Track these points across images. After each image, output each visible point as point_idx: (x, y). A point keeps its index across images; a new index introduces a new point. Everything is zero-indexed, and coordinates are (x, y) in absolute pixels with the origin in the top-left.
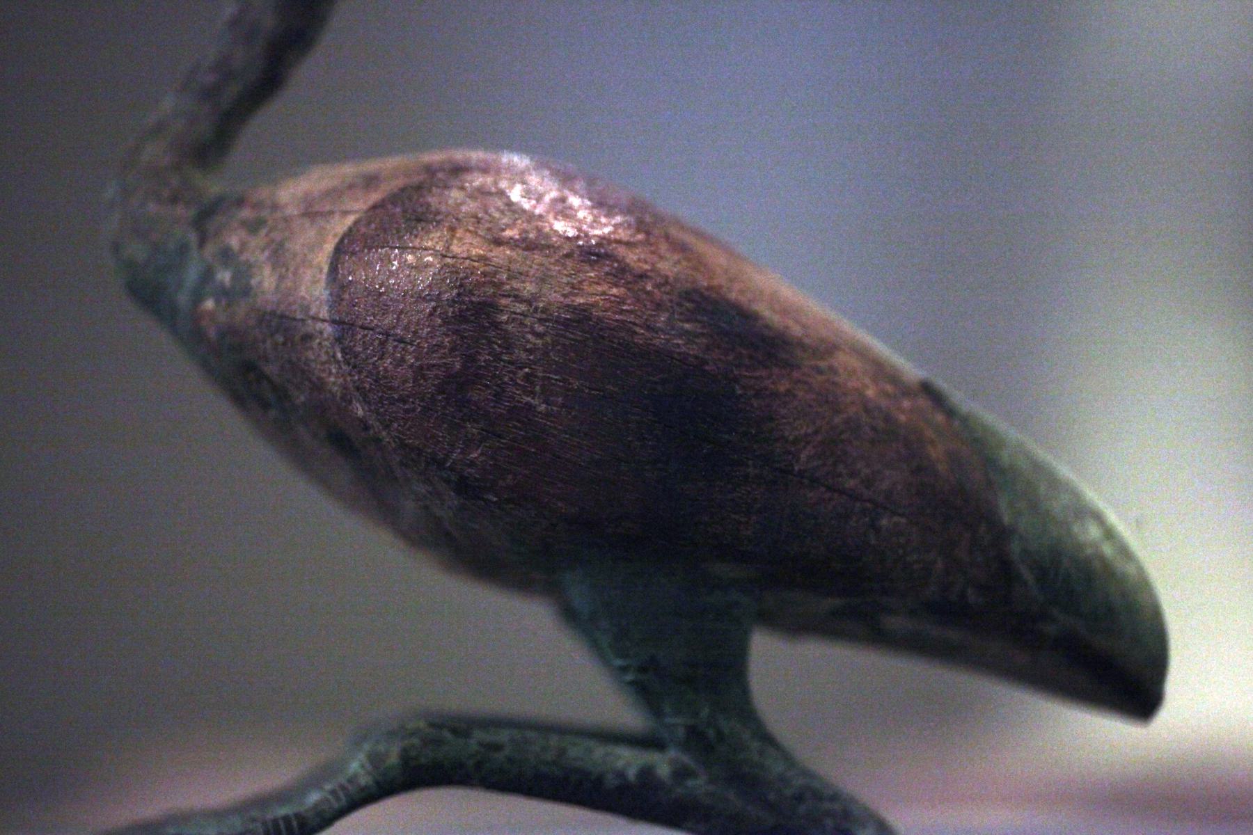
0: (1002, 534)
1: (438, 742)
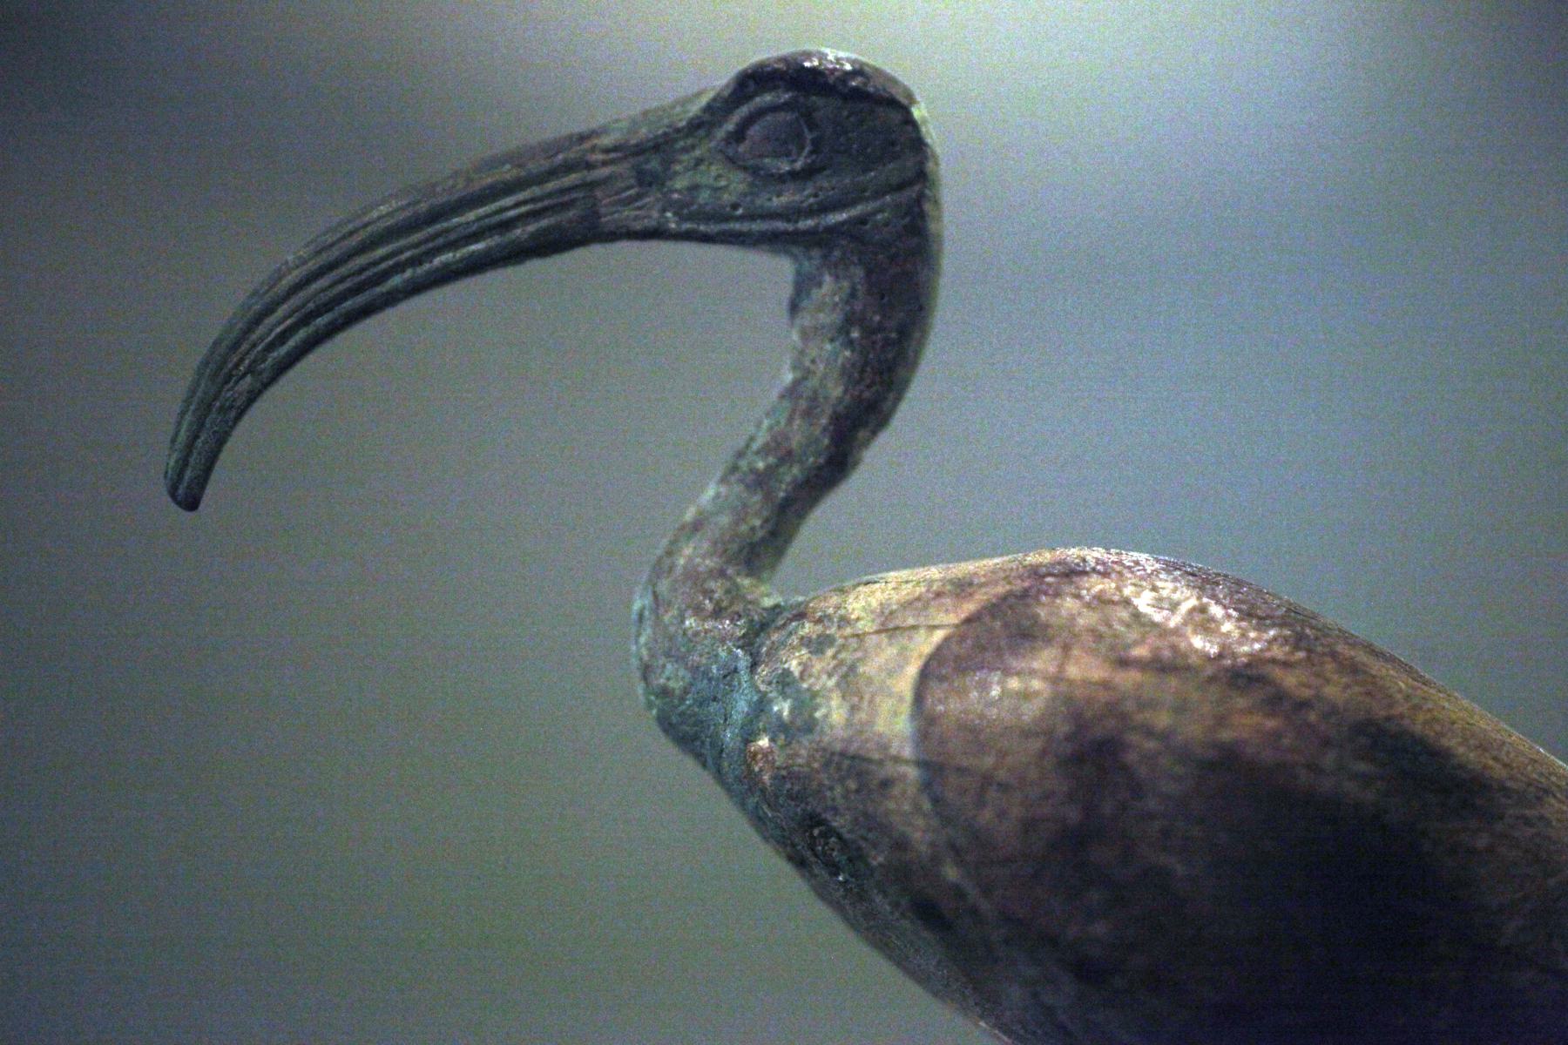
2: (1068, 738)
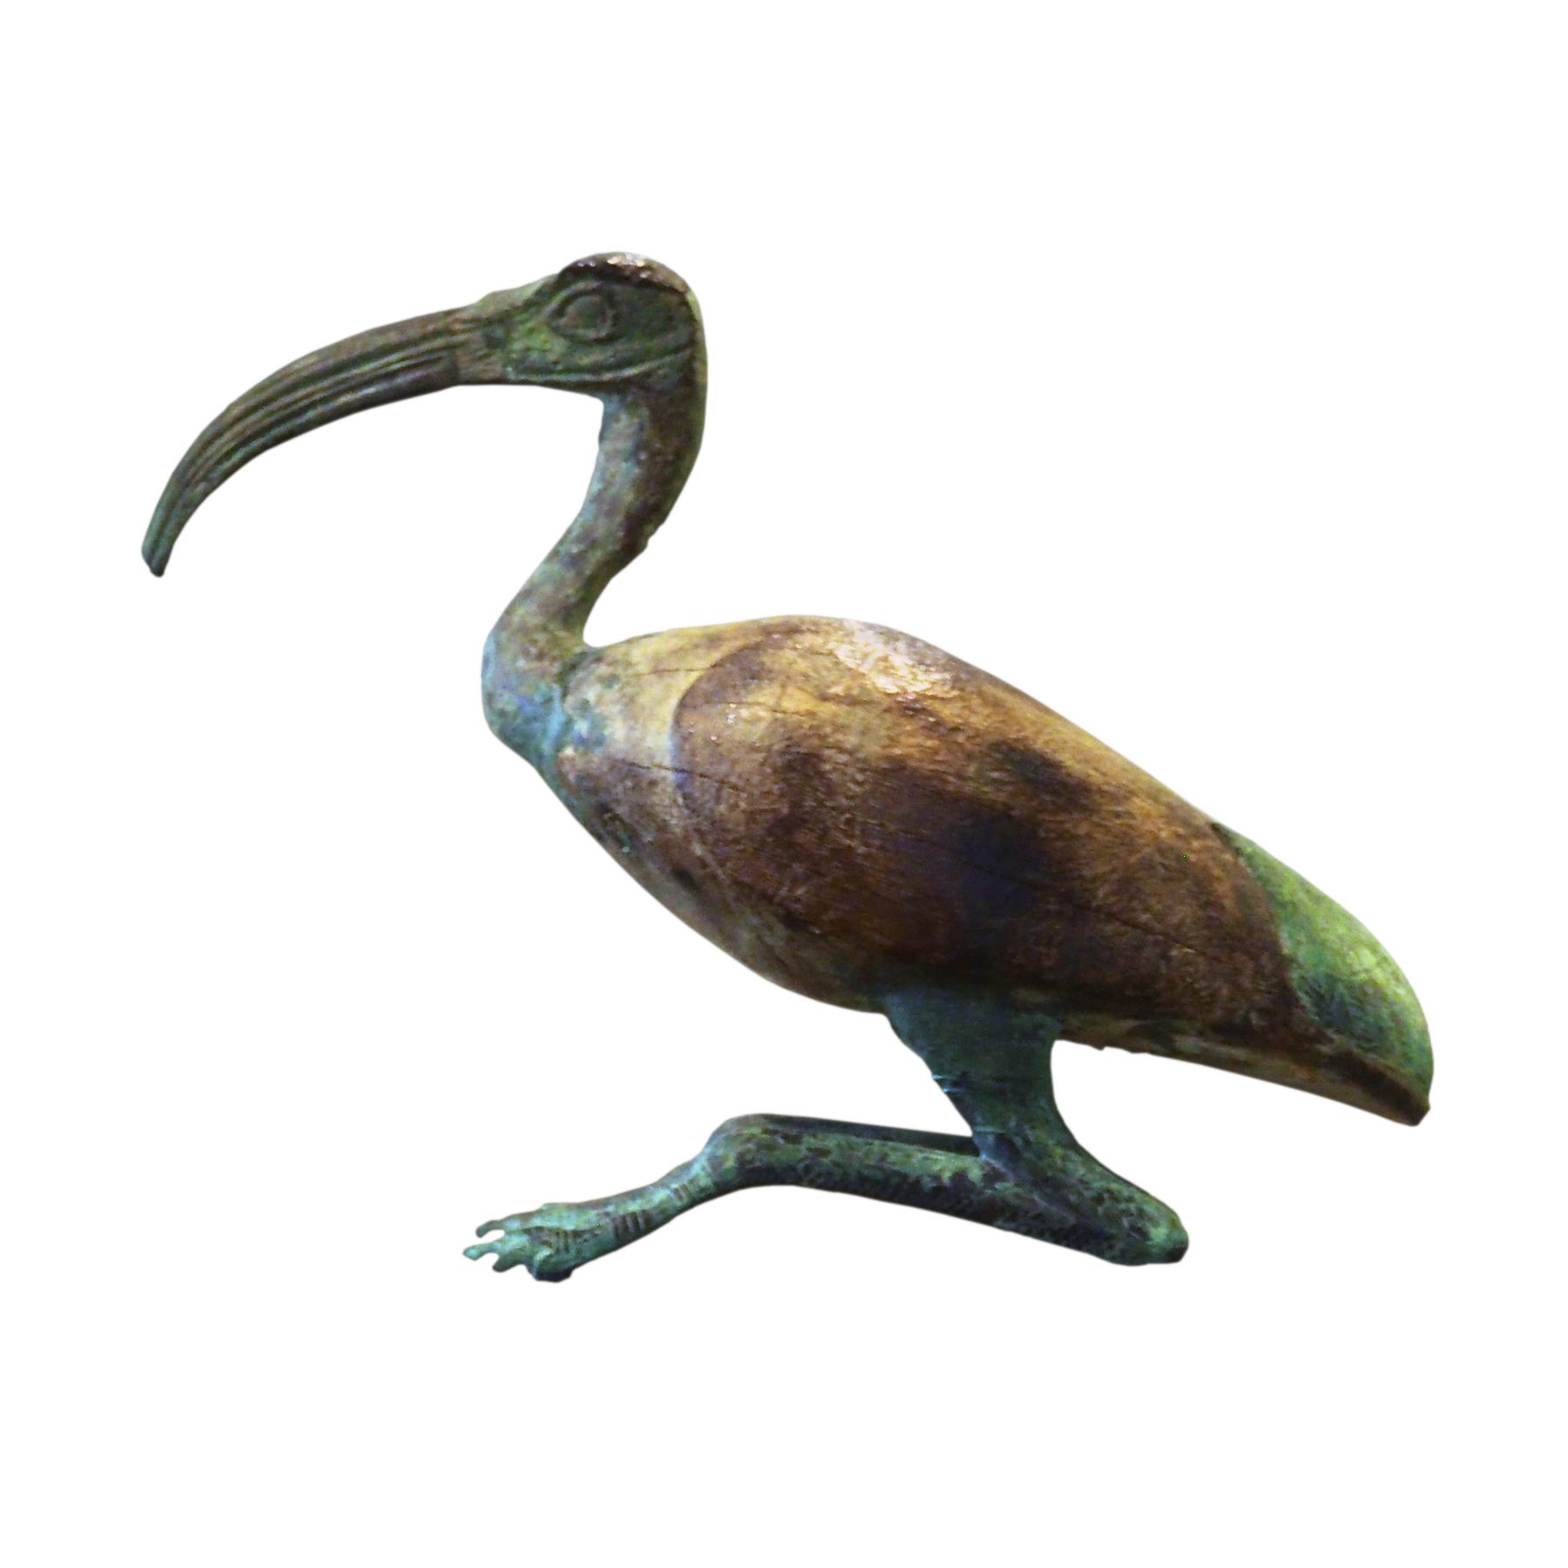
0: (1283, 963)
1: (770, 1147)
2: (782, 753)
